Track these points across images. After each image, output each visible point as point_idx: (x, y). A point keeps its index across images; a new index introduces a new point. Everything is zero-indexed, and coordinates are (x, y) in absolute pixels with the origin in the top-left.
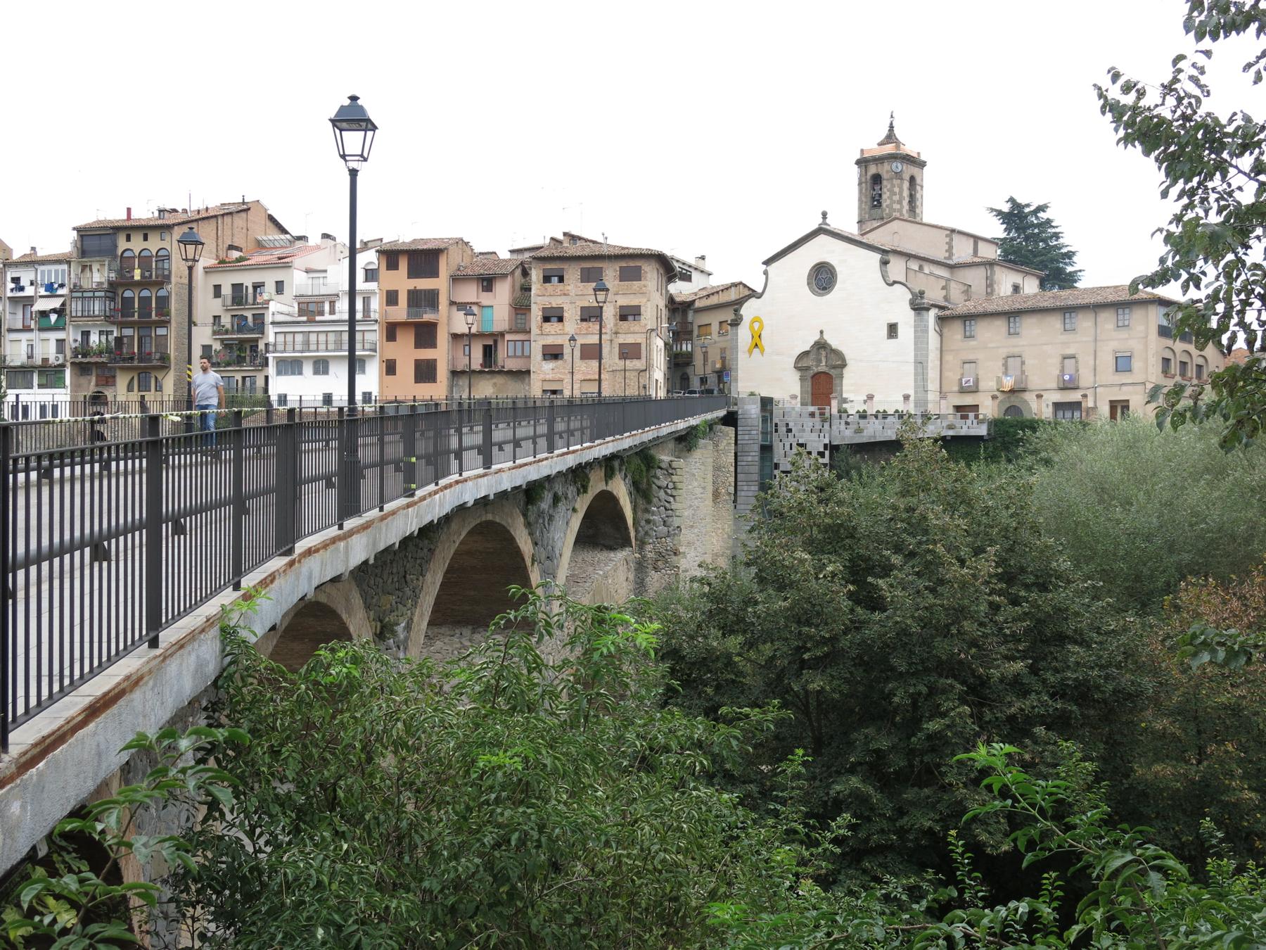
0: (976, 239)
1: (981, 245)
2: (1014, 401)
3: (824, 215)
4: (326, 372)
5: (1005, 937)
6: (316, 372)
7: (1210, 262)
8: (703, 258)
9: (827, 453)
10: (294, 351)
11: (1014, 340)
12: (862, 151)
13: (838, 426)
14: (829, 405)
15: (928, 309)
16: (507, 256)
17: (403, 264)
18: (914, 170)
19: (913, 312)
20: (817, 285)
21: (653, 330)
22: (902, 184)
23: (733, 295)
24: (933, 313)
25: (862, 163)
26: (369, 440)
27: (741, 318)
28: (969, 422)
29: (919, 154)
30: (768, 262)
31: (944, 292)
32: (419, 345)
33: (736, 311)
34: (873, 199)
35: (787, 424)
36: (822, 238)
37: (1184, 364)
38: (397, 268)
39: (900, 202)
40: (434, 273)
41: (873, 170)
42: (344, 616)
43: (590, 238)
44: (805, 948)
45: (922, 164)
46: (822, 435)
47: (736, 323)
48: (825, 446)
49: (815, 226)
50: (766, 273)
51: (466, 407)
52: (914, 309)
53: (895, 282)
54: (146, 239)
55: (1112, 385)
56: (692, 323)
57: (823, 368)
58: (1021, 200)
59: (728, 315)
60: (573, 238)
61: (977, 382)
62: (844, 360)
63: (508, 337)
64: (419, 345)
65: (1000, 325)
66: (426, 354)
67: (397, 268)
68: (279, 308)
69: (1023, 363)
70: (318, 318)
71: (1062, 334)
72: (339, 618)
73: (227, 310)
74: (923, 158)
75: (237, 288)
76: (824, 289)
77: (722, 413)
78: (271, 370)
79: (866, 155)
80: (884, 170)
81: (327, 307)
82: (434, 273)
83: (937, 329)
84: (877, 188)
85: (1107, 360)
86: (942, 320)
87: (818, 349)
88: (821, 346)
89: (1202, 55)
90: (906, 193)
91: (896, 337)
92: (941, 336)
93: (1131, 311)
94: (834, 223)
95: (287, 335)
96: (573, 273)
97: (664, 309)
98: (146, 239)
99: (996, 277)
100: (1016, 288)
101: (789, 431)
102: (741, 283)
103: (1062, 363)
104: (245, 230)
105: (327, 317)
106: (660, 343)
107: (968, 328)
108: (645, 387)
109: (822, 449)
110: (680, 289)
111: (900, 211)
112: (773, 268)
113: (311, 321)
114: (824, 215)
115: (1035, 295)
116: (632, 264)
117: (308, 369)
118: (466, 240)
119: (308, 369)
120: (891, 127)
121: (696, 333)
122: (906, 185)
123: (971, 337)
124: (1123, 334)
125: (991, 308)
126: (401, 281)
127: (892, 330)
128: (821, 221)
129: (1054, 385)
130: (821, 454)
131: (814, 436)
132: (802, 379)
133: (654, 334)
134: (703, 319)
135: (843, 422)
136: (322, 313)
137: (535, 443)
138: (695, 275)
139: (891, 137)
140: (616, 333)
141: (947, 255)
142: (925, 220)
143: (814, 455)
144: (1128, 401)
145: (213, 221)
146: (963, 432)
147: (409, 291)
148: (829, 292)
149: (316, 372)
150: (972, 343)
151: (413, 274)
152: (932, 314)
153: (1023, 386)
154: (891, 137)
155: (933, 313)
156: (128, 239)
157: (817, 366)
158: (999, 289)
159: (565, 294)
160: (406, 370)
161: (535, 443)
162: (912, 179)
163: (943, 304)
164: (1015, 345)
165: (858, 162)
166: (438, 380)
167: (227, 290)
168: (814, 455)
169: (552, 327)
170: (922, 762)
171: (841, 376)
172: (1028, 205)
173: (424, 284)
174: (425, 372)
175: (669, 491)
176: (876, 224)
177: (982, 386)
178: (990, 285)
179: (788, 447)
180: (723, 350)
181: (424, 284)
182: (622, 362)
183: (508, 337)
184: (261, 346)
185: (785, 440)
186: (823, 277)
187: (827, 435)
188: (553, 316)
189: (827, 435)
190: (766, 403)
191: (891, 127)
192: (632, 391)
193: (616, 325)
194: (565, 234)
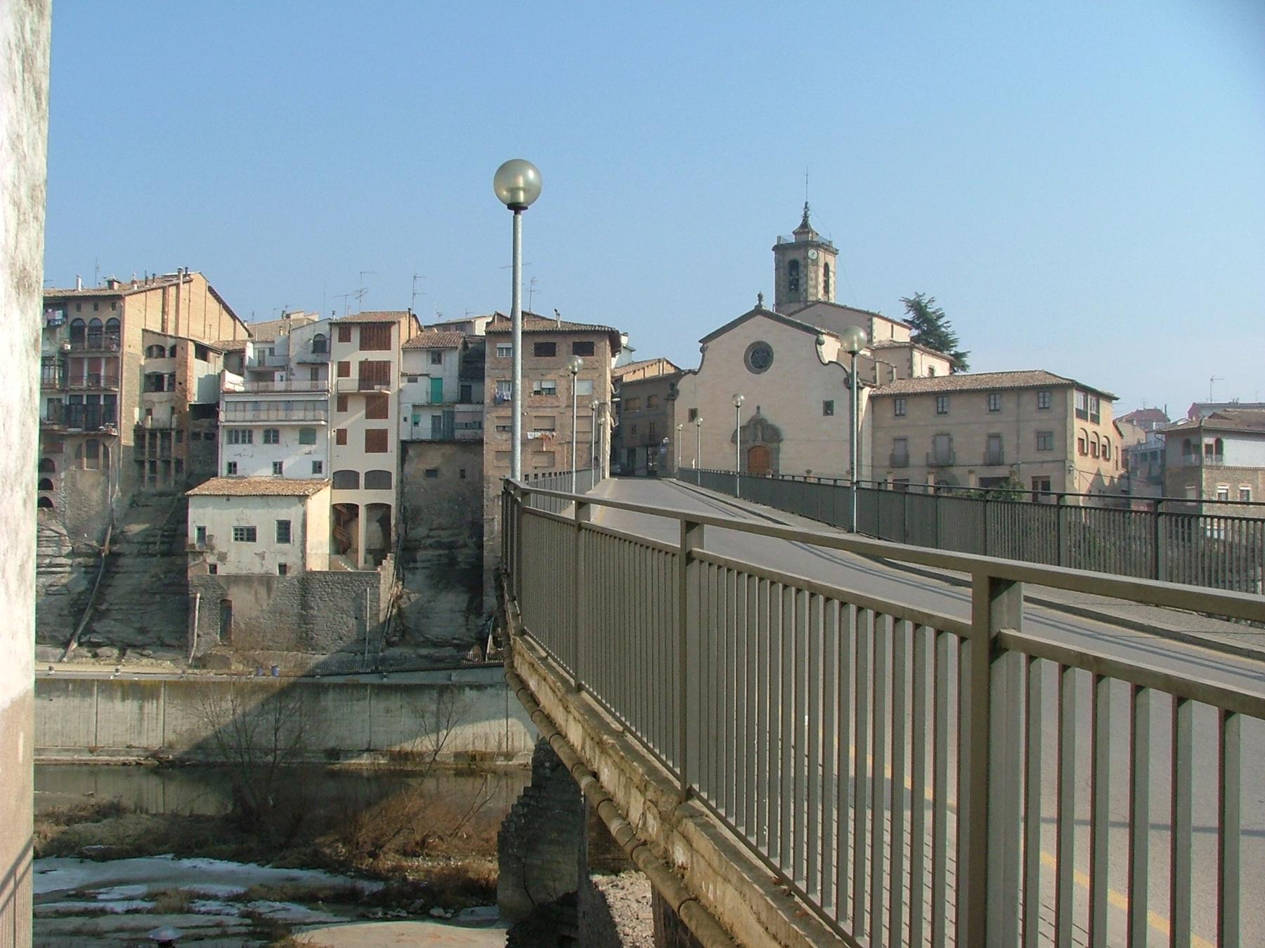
4: (276, 441)
5: (324, 649)
12: (779, 238)
17: (355, 335)
18: (831, 260)
25: (779, 249)
27: (677, 392)
32: (370, 415)
34: (791, 283)
36: (759, 317)
37: (1081, 440)
38: (349, 340)
39: (816, 287)
40: (386, 346)
50: (702, 350)
54: (96, 308)
55: (1035, 462)
61: (907, 456)
64: (370, 415)
66: (377, 424)
67: (349, 340)
69: (951, 440)
71: (987, 414)
76: (761, 367)
82: (386, 346)
85: (1029, 438)
89: (800, 222)
90: (821, 279)
91: (832, 414)
98: (96, 308)
100: (932, 370)
103: (934, 442)
104: (187, 302)
107: (940, 405)
112: (711, 344)
117: (258, 437)
119: (258, 437)
120: (806, 217)
122: (821, 271)
124: (1044, 416)
127: (828, 408)
129: (981, 462)
139: (805, 225)
144: (1049, 477)
147: (361, 363)
148: (766, 370)
149: (267, 441)
150: (903, 421)
153: (951, 462)
154: (805, 225)
156: (79, 309)
157: (754, 441)
160: (357, 440)
165: (776, 248)
171: (778, 450)
173: (375, 356)
177: (912, 460)
180: (652, 425)
181: (375, 356)
191: (806, 217)
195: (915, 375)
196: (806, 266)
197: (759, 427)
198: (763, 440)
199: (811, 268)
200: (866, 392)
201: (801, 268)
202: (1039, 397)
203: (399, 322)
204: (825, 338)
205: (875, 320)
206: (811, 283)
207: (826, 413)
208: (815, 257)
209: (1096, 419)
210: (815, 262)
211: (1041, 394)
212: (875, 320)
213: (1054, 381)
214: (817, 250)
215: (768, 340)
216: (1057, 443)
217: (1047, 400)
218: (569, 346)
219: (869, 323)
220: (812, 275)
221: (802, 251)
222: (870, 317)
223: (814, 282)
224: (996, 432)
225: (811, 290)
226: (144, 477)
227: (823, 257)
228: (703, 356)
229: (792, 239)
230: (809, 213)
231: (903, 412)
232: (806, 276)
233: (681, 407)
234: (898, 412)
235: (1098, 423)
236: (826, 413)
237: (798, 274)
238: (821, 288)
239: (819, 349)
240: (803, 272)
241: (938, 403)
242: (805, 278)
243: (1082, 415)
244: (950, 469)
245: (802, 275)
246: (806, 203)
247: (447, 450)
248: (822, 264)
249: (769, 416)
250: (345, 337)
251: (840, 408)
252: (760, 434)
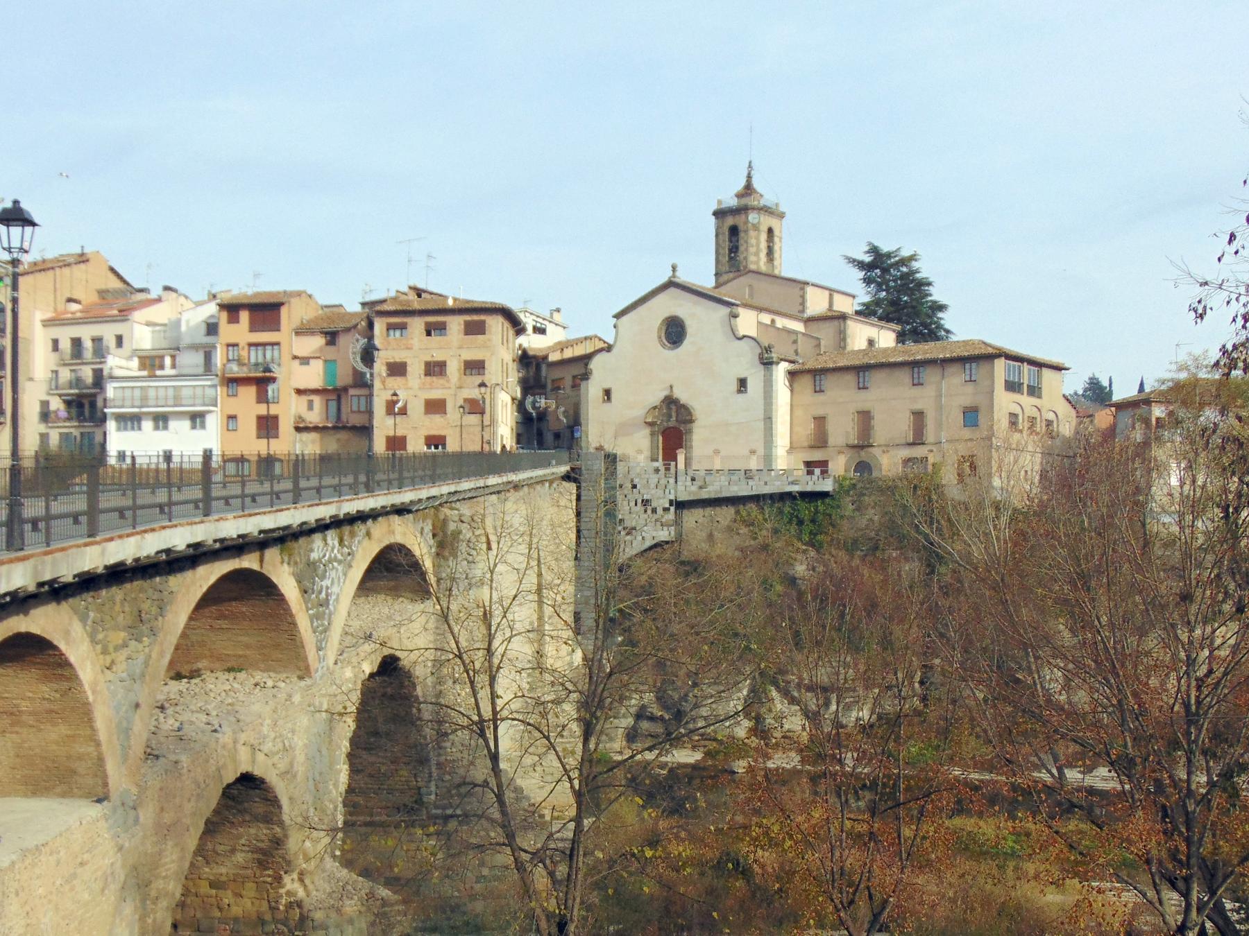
0: (832, 291)
1: (836, 297)
2: (864, 455)
3: (674, 268)
4: (166, 428)
6: (157, 428)
9: (672, 509)
10: (133, 407)
11: (863, 394)
12: (719, 202)
14: (675, 460)
16: (358, 308)
17: (244, 316)
24: (783, 367)
25: (719, 214)
26: (673, 533)
29: (777, 205)
30: (618, 316)
31: (794, 347)
35: (632, 481)
36: (672, 290)
39: (757, 254)
41: (730, 221)
42: (63, 646)
43: (435, 291)
44: (349, 930)
45: (781, 216)
46: (667, 491)
47: (586, 376)
48: (671, 503)
49: (663, 279)
51: (300, 458)
56: (546, 378)
57: (673, 422)
58: (885, 248)
59: (577, 370)
60: (419, 293)
62: (690, 414)
63: (352, 392)
68: (119, 364)
70: (159, 373)
72: (55, 648)
73: (65, 365)
74: (782, 209)
75: (77, 343)
77: (564, 469)
78: (111, 425)
79: (724, 206)
81: (168, 361)
83: (787, 383)
86: (792, 375)
88: (670, 402)
89: (743, 183)
90: (763, 245)
91: (746, 391)
94: (683, 277)
95: (126, 390)
96: (417, 325)
97: (510, 363)
99: (849, 332)
100: (871, 342)
101: (634, 487)
102: (596, 337)
105: (168, 371)
107: (818, 383)
108: (489, 443)
109: (667, 505)
110: (532, 342)
113: (152, 376)
114: (674, 268)
115: (894, 349)
116: (475, 318)
117: (147, 425)
118: (309, 293)
119: (147, 425)
120: (749, 177)
122: (764, 237)
126: (241, 332)
127: (742, 383)
128: (671, 273)
130: (666, 510)
131: (660, 492)
132: (652, 434)
133: (498, 389)
135: (689, 479)
136: (162, 367)
137: (181, 479)
138: (550, 328)
139: (748, 189)
140: (461, 387)
141: (801, 308)
142: (786, 273)
143: (660, 511)
145: (50, 273)
146: (809, 488)
148: (677, 347)
149: (157, 428)
151: (253, 328)
152: (781, 370)
154: (748, 189)
159: (408, 348)
160: (248, 425)
161: (181, 479)
162: (770, 231)
163: (793, 357)
164: (866, 400)
166: (384, 440)
167: (65, 345)
168: (660, 511)
169: (395, 383)
170: (732, 819)
171: (690, 432)
174: (268, 426)
175: (471, 545)
176: (731, 275)
178: (842, 338)
179: (632, 504)
182: (272, 412)
183: (352, 392)
184: (100, 403)
186: (674, 332)
187: (672, 491)
188: (397, 369)
189: (672, 491)
190: (611, 459)
191: (749, 177)
192: (474, 447)
193: (460, 379)
194: (410, 288)
195: (849, 348)
196: (746, 231)
197: (673, 407)
198: (677, 421)
199: (752, 233)
201: (742, 235)
203: (289, 302)
204: (741, 311)
206: (752, 250)
207: (739, 391)
208: (755, 221)
209: (1034, 391)
210: (756, 228)
211: (916, 370)
213: (990, 350)
214: (759, 213)
216: (982, 419)
218: (459, 324)
220: (753, 241)
221: (743, 216)
225: (752, 258)
227: (766, 221)
231: (921, 381)
232: (746, 242)
233: (593, 390)
234: (916, 381)
235: (1040, 397)
236: (739, 391)
238: (763, 255)
243: (1012, 387)
244: (870, 449)
245: (741, 242)
246: (750, 162)
247: (343, 435)
248: (764, 228)
249: (682, 395)
250: (233, 319)
251: (755, 385)
252: (674, 414)
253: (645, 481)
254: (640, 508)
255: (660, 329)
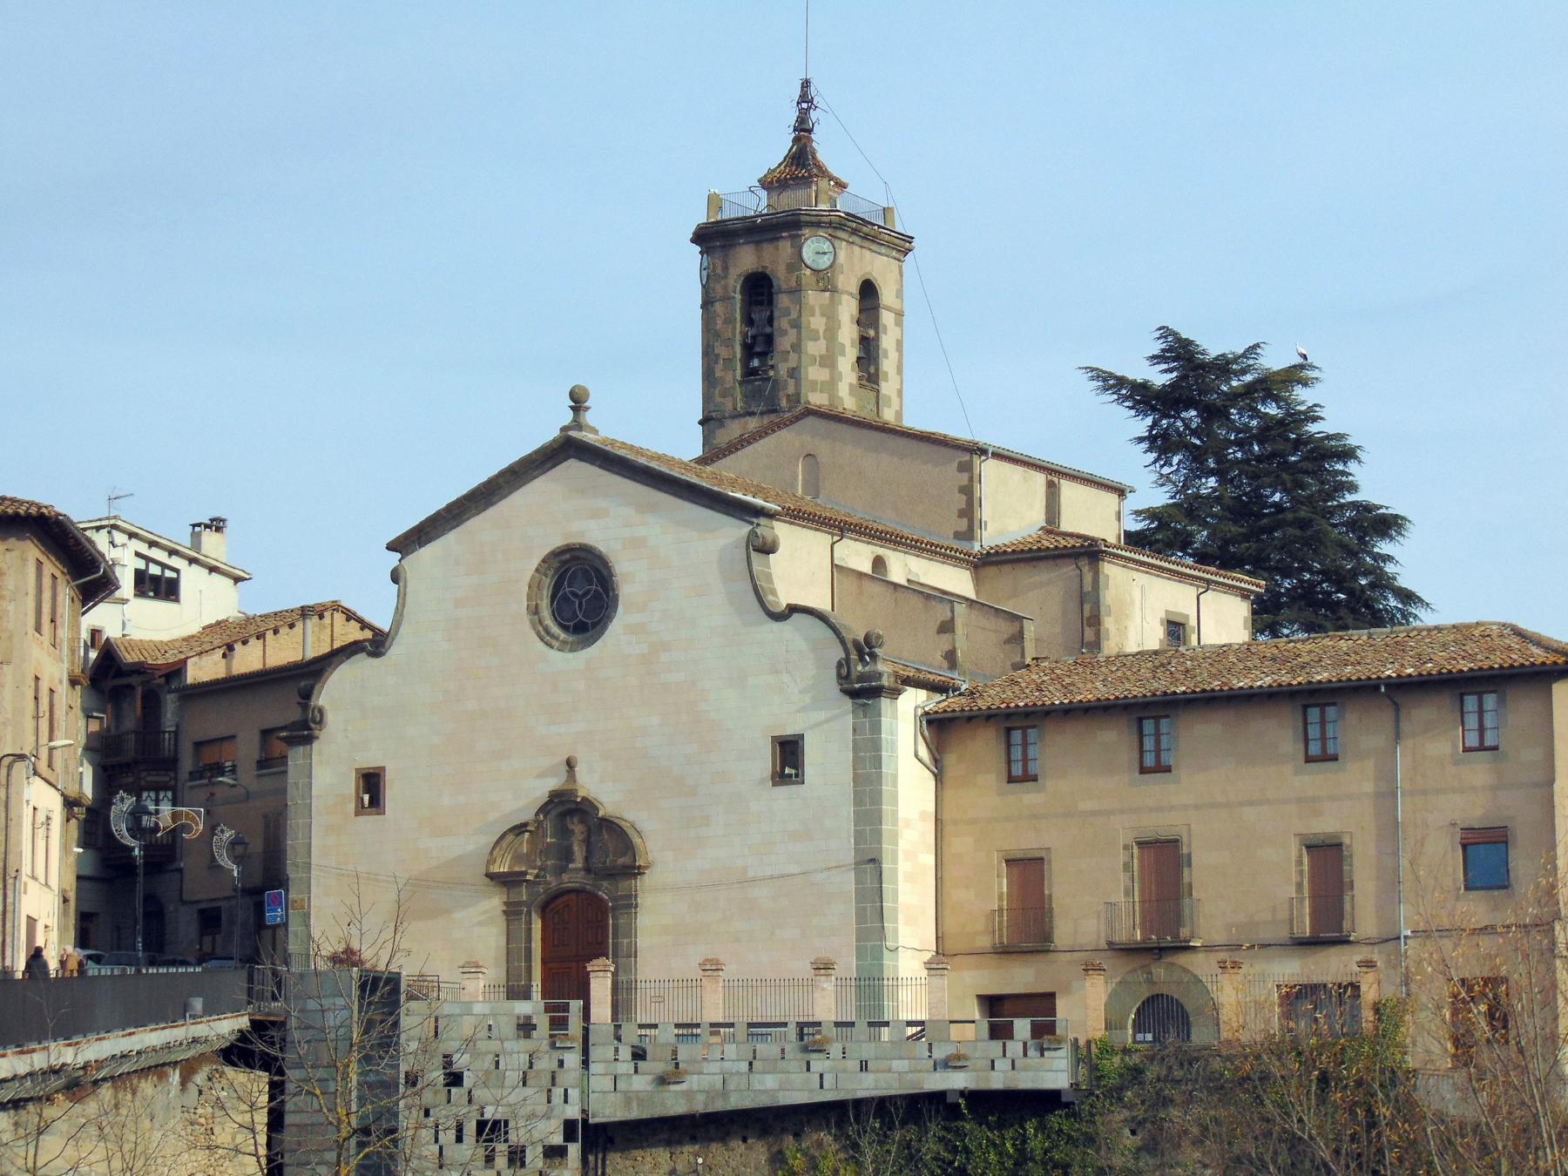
0: (1054, 475)
1: (1068, 489)
3: (578, 401)
7: (586, 404)
8: (217, 525)
9: (574, 1150)
11: (1155, 789)
12: (714, 202)
13: (609, 1060)
14: (584, 993)
15: (895, 693)
18: (878, 265)
19: (847, 703)
20: (557, 614)
21: (22, 757)
22: (833, 303)
23: (308, 643)
28: (1014, 1047)
30: (405, 544)
31: (944, 643)
33: (307, 695)
36: (573, 468)
39: (829, 361)
41: (746, 259)
45: (902, 245)
46: (558, 1092)
48: (570, 1128)
49: (546, 433)
50: (396, 577)
52: (853, 694)
53: (793, 609)
57: (574, 877)
65: (1114, 739)
77: (228, 1026)
79: (727, 214)
80: (775, 258)
83: (924, 752)
84: (759, 315)
86: (938, 727)
87: (563, 815)
89: (780, 147)
90: (848, 334)
91: (798, 778)
92: (939, 778)
93: (1502, 701)
97: (63, 689)
99: (1109, 596)
100: (1175, 629)
101: (455, 1079)
102: (336, 607)
106: (51, 802)
111: (831, 386)
114: (578, 401)
120: (803, 129)
121: (187, 764)
122: (848, 308)
123: (1028, 778)
125: (1091, 690)
127: (789, 753)
128: (568, 417)
129: (984, 942)
131: (533, 1096)
132: (512, 912)
133: (20, 768)
134: (209, 722)
141: (963, 525)
142: (912, 422)
146: (997, 1081)
155: (913, 701)
157: (561, 870)
158: (1123, 631)
162: (868, 291)
163: (942, 674)
168: (534, 1157)
171: (628, 904)
172: (1303, 403)
176: (753, 424)
185: (440, 1113)
187: (574, 1094)
189: (574, 1094)
191: (803, 129)
195: (1110, 647)
196: (796, 291)
198: (588, 870)
199: (813, 298)
200: (913, 701)
201: (783, 301)
202: (1009, 746)
204: (782, 531)
205: (990, 470)
206: (814, 348)
207: (780, 778)
208: (824, 262)
210: (826, 280)
211: (1314, 714)
212: (990, 470)
215: (597, 534)
217: (1489, 721)
219: (965, 477)
220: (817, 322)
222: (966, 457)
223: (822, 343)
224: (1330, 829)
225: (814, 373)
226: (146, 915)
227: (856, 263)
228: (402, 597)
229: (756, 204)
230: (813, 115)
232: (796, 325)
236: (780, 778)
237: (770, 321)
239: (756, 568)
240: (787, 312)
241: (1009, 746)
242: (793, 333)
245: (782, 323)
246: (806, 84)
248: (849, 284)
249: (595, 785)
252: (579, 852)
253: (488, 1062)
254: (469, 1148)
255: (535, 586)
